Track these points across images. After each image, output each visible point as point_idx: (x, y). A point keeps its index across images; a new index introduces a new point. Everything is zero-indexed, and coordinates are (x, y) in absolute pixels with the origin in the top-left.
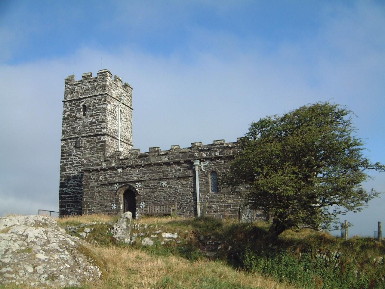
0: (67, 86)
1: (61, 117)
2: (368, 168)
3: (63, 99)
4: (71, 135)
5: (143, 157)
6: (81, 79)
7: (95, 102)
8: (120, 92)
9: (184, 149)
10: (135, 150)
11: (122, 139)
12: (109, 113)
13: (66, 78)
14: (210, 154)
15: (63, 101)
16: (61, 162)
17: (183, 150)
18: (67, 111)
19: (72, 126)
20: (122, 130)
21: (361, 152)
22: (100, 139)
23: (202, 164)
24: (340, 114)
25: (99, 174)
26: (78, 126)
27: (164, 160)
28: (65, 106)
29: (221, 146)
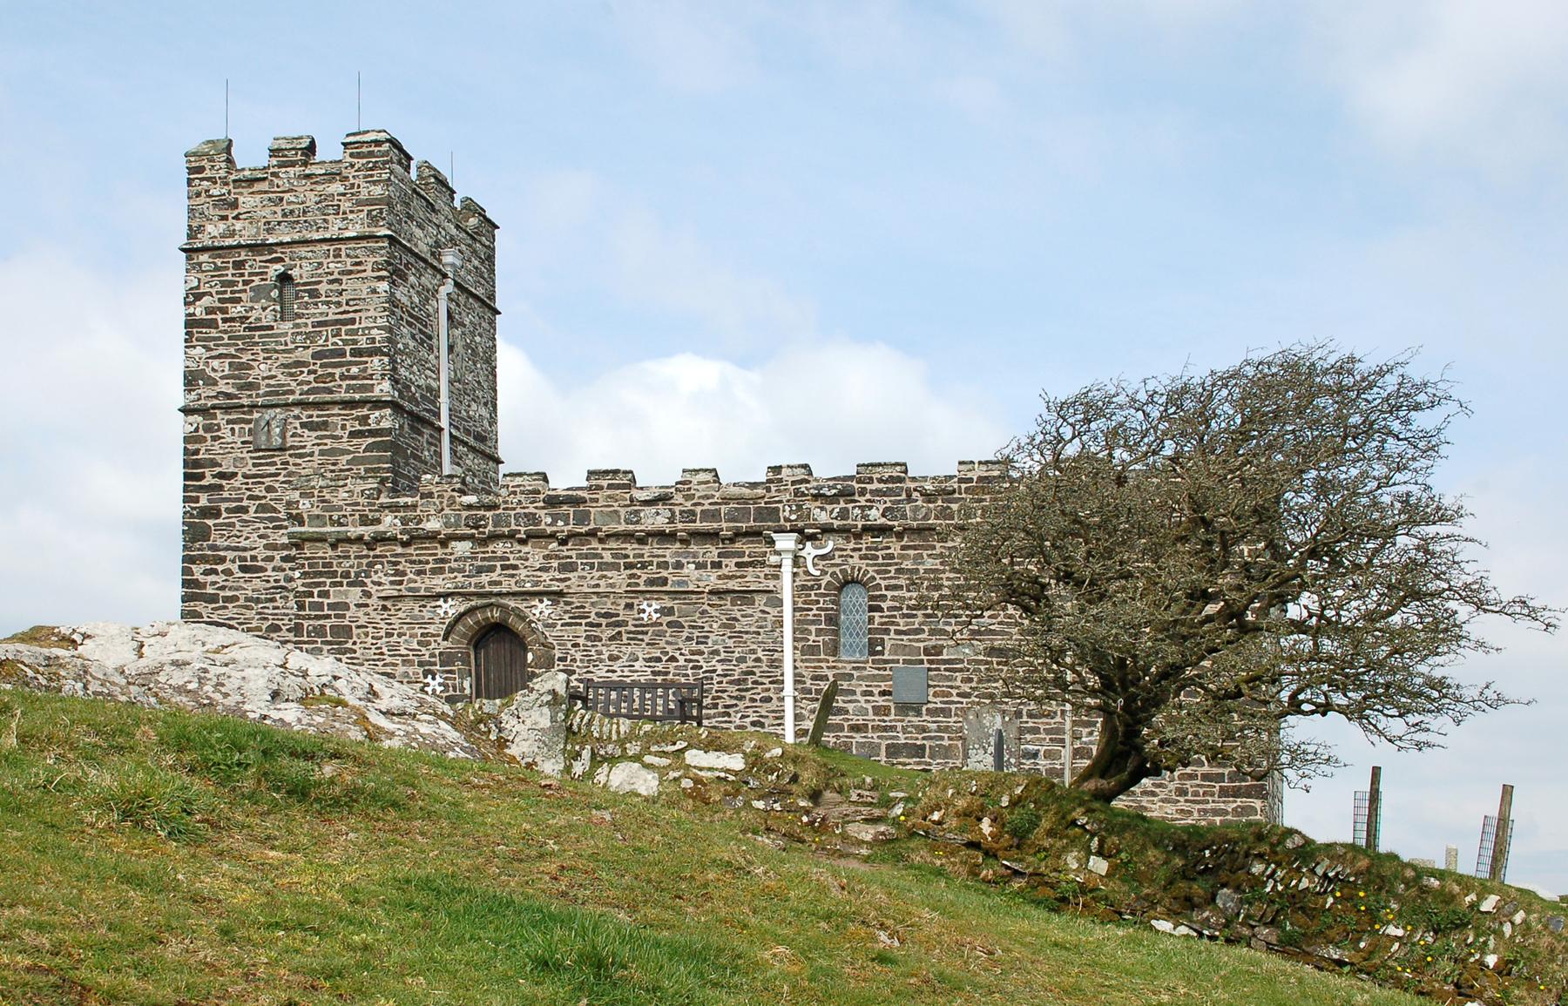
0: (197, 182)
1: (179, 314)
2: (1485, 611)
3: (183, 240)
4: (228, 396)
5: (562, 503)
6: (263, 159)
7: (339, 265)
8: (443, 233)
9: (734, 485)
10: (525, 474)
11: (458, 429)
12: (402, 319)
13: (192, 146)
14: (844, 514)
15: (184, 250)
16: (186, 500)
17: (736, 491)
18: (204, 294)
19: (234, 356)
20: (456, 391)
21: (1465, 552)
22: (364, 420)
23: (810, 551)
24: (1406, 401)
25: (368, 556)
26: (260, 359)
27: (650, 521)
28: (194, 267)
29: (890, 486)
